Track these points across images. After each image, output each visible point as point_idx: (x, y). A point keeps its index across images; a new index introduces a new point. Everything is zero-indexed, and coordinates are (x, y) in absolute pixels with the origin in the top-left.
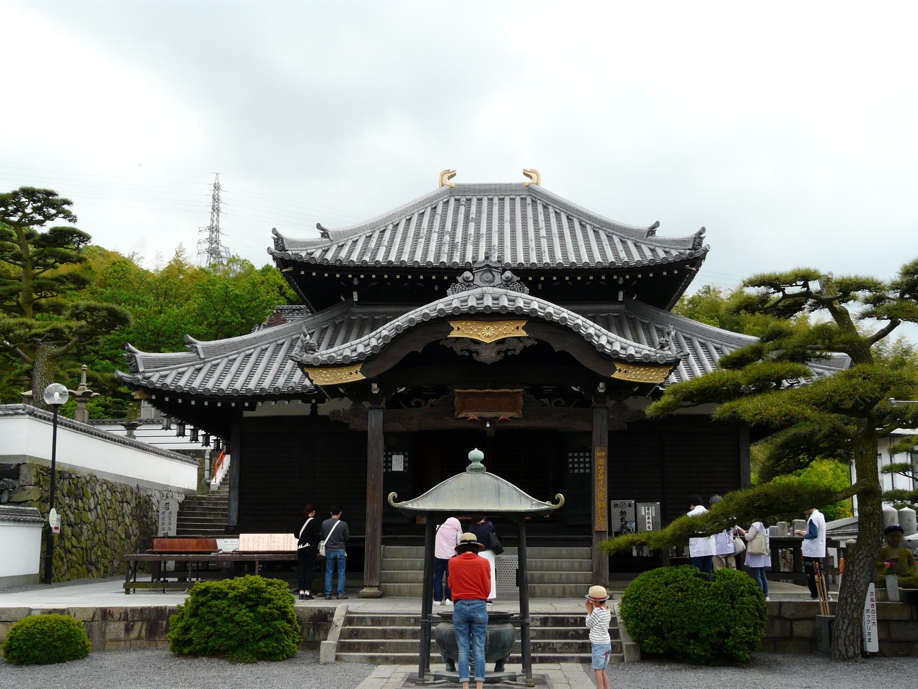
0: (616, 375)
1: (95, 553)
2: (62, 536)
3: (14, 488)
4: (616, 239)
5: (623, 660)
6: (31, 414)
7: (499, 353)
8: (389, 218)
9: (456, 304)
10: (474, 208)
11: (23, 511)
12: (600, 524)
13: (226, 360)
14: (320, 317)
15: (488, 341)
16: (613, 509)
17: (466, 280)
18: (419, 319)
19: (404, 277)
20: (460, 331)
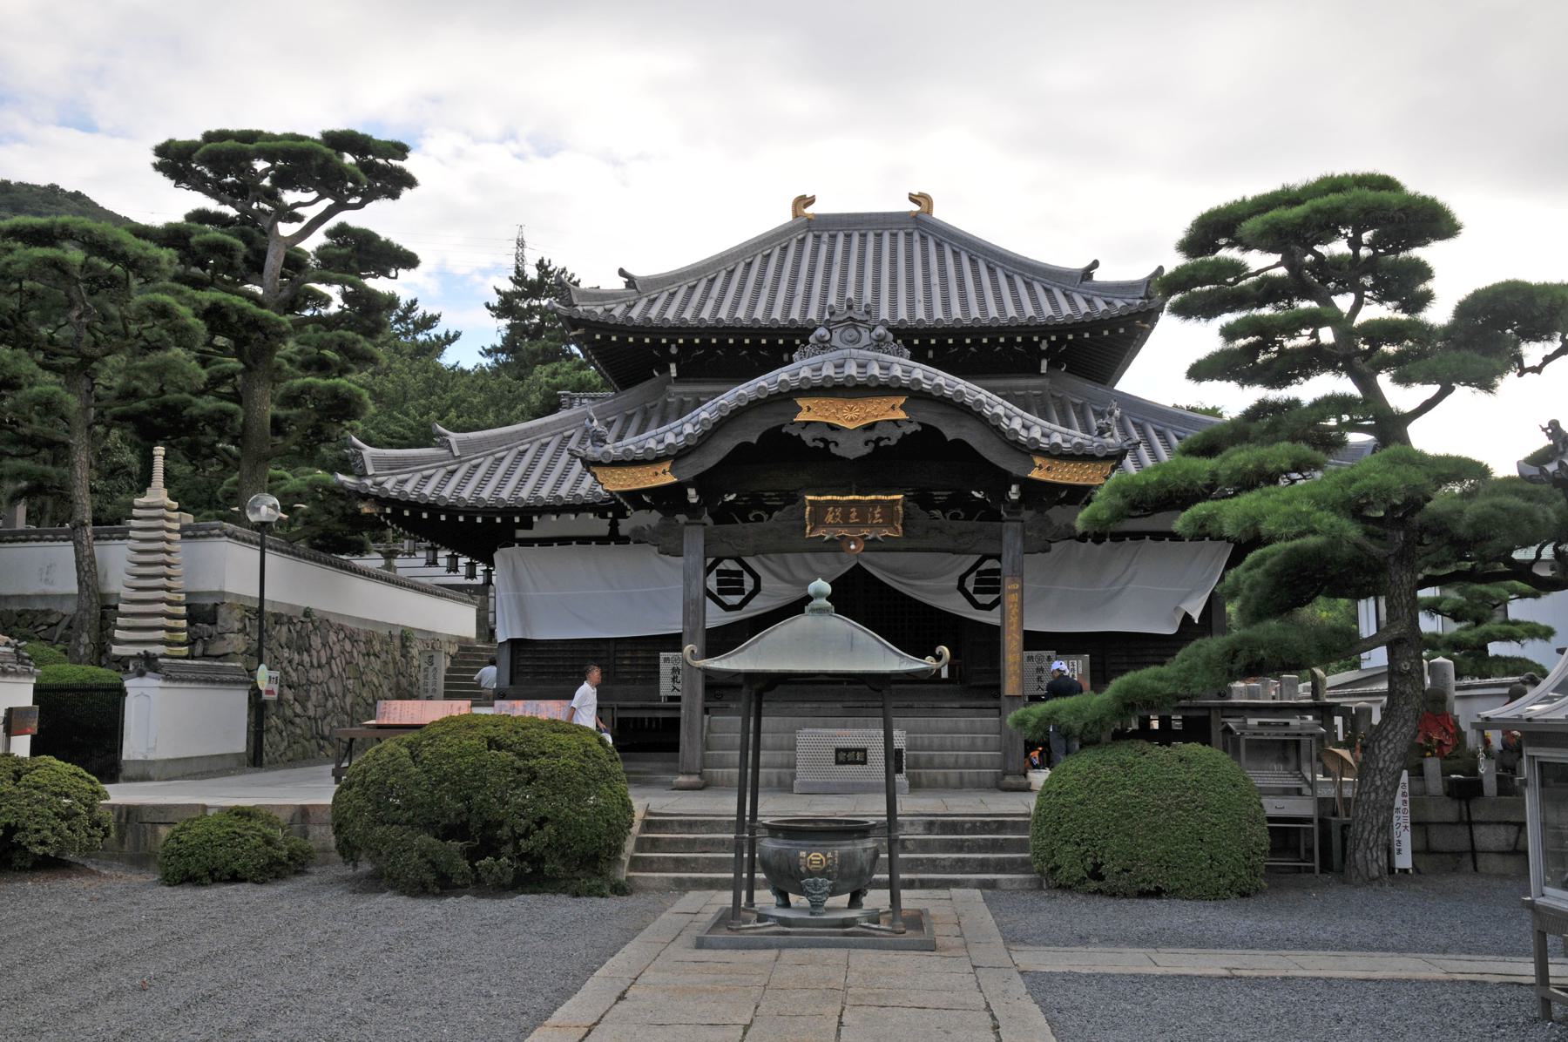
0: (1035, 474)
12: (1011, 686)
13: (491, 459)
15: (851, 426)
17: (821, 340)
18: (753, 396)
20: (810, 411)
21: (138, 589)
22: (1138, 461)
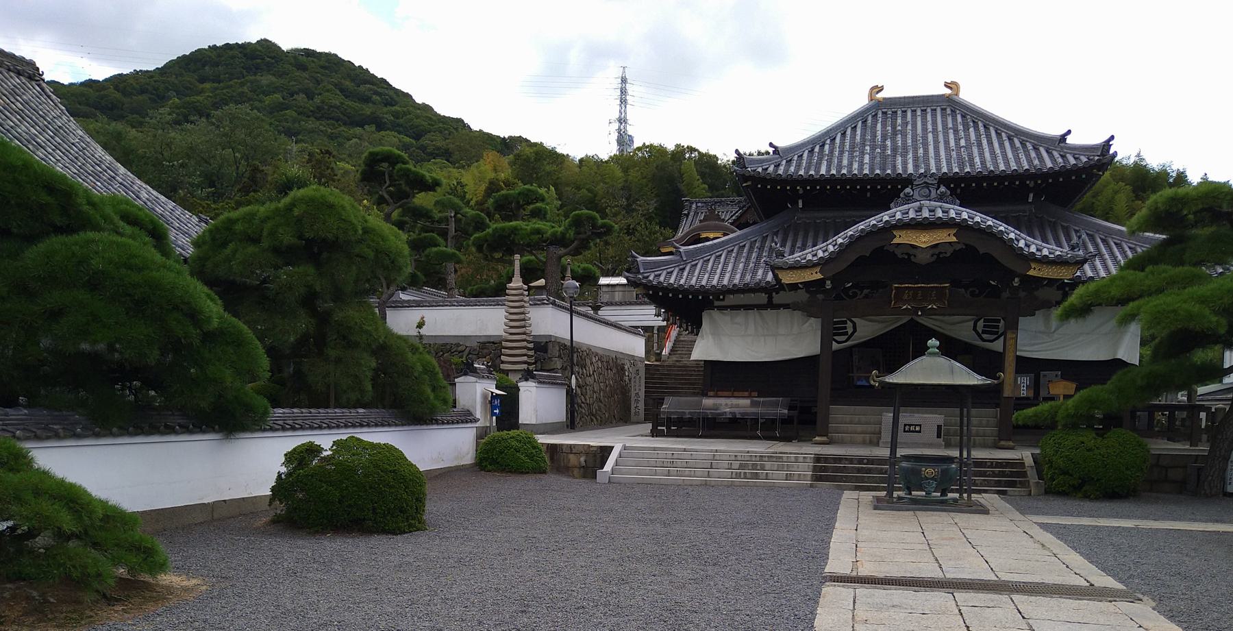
4: (1030, 147)
6: (554, 304)
9: (899, 216)
14: (771, 222)
15: (924, 246)
17: (907, 195)
19: (843, 188)
20: (901, 238)
22: (1094, 268)
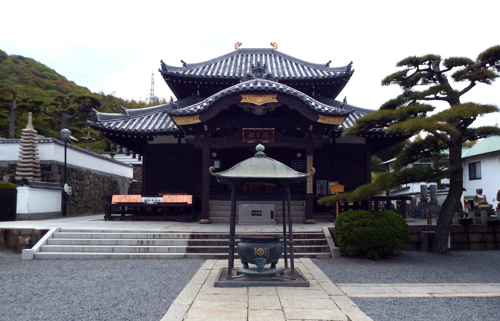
0: (319, 121)
1: (90, 203)
2: (73, 195)
3: (49, 174)
5: (331, 256)
6: (55, 142)
7: (264, 110)
8: (213, 60)
9: (244, 86)
10: (249, 58)
11: (51, 185)
13: (139, 118)
15: (259, 104)
16: (317, 184)
20: (246, 99)
21: (24, 158)
